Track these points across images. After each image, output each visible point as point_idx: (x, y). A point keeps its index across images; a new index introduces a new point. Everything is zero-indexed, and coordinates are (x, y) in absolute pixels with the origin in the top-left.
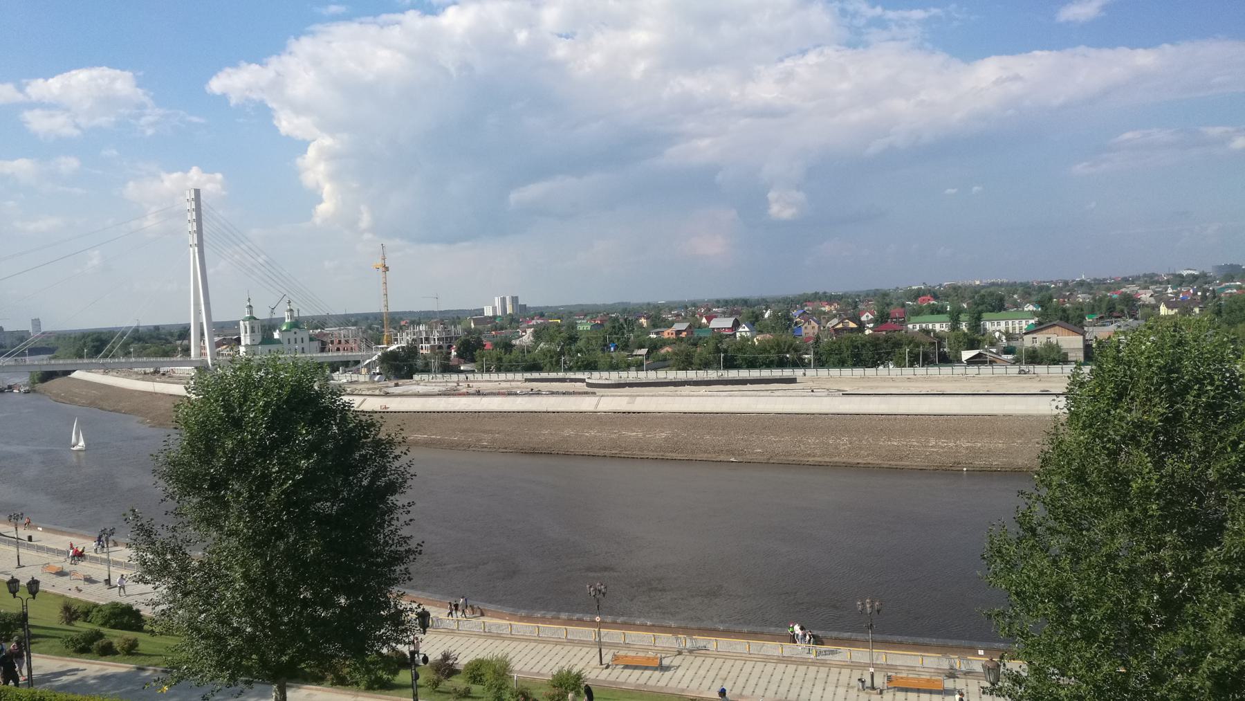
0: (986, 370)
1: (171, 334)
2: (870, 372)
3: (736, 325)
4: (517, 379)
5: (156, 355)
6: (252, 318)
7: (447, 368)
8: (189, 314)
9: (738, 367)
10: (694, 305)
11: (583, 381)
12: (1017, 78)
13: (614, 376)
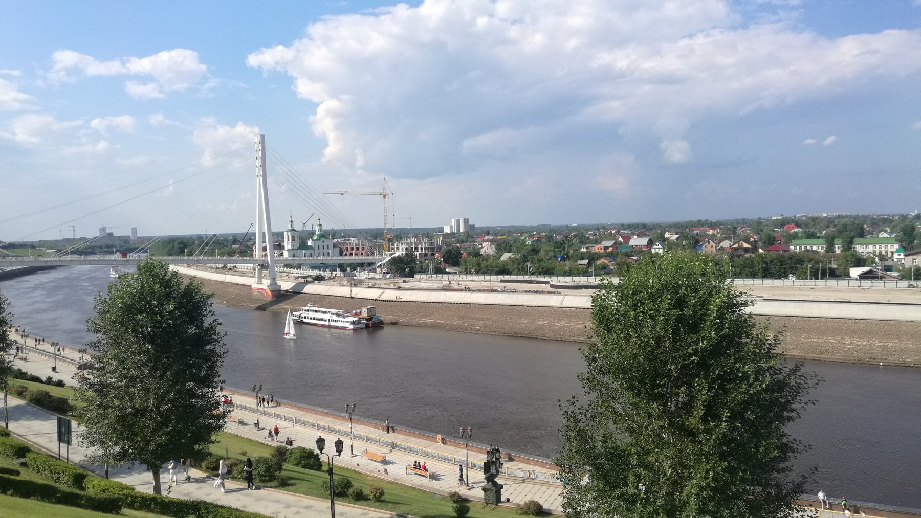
0: (878, 284)
1: (226, 240)
2: (778, 282)
3: (651, 243)
4: (494, 280)
5: (223, 254)
6: (292, 230)
7: (439, 271)
8: (258, 228)
9: (525, 274)
10: (604, 227)
11: (547, 283)
12: (874, 52)
13: (569, 281)
